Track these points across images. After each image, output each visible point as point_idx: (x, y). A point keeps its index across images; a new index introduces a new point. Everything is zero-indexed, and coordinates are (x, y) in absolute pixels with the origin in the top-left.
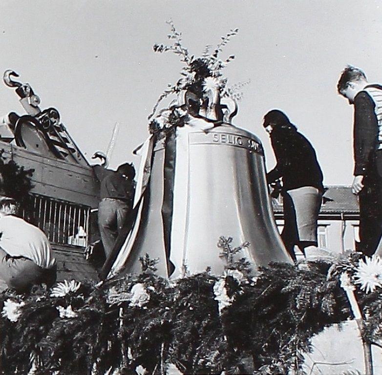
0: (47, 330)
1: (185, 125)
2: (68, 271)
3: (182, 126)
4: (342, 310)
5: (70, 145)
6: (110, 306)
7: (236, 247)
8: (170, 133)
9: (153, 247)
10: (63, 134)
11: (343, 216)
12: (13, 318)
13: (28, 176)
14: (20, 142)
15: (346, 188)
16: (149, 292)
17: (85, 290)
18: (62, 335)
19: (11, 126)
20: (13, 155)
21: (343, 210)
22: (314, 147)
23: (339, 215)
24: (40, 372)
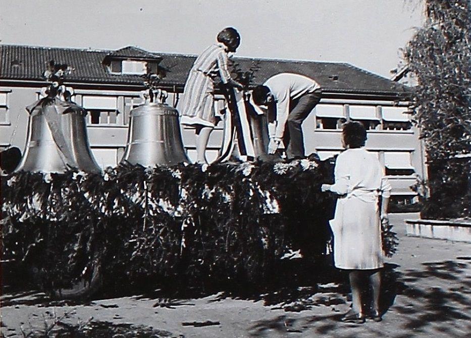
1: (177, 108)
4: (36, 197)
7: (62, 107)
15: (185, 57)
21: (176, 82)
22: (335, 261)
23: (171, 87)
24: (426, 86)
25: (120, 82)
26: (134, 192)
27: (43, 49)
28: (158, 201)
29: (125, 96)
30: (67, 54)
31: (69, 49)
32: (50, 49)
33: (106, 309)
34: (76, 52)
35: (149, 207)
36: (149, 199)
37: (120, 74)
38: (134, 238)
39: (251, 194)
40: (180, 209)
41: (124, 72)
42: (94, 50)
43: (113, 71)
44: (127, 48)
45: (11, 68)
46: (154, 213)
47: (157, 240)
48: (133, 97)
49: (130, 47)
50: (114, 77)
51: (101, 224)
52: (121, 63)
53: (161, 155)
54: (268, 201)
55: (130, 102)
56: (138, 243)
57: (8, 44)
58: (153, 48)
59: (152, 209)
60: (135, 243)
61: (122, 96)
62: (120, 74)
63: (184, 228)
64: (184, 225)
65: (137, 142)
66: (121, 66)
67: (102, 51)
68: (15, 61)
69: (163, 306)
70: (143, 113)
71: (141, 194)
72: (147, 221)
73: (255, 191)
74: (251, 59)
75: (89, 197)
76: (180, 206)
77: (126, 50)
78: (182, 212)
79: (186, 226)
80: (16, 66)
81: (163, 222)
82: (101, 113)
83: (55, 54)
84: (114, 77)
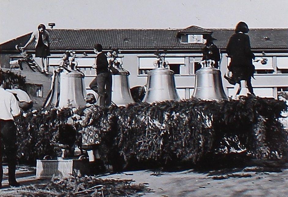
0: (31, 119)
2: (36, 103)
3: (61, 72)
5: (36, 65)
6: (267, 119)
8: (59, 74)
9: (55, 102)
10: (34, 62)
11: (220, 51)
12: (25, 116)
13: (24, 78)
14: (22, 69)
15: (228, 30)
16: (48, 112)
17: (38, 111)
18: (34, 119)
19: (19, 64)
20: (20, 73)
25: (187, 48)
26: (142, 116)
27: (142, 30)
28: (153, 121)
29: (189, 57)
30: (156, 32)
31: (157, 30)
32: (146, 30)
33: (127, 176)
34: (162, 31)
35: (149, 124)
36: (149, 120)
37: (186, 43)
38: (141, 140)
39: (199, 117)
40: (164, 125)
41: (189, 42)
42: (172, 30)
43: (182, 42)
44: (191, 27)
45: (123, 43)
46: (151, 127)
47: (152, 142)
48: (194, 57)
49: (193, 26)
50: (183, 45)
51: (126, 133)
52: (188, 36)
53: (214, 94)
54: (207, 121)
55: (193, 60)
56: (143, 143)
57: (126, 28)
58: (206, 26)
59: (151, 125)
60: (141, 143)
61: (188, 57)
62: (186, 43)
63: (162, 134)
64: (162, 133)
65: (150, 89)
66: (187, 38)
67: (177, 30)
68: (126, 38)
69: (155, 175)
70: (153, 74)
71: (145, 117)
72: (148, 131)
73: (201, 115)
74: (272, 29)
75: (121, 118)
76: (164, 124)
77: (190, 28)
78: (165, 127)
79: (163, 133)
80: (127, 41)
81: (156, 132)
82: (181, 65)
83: (121, 45)
84: (183, 45)
